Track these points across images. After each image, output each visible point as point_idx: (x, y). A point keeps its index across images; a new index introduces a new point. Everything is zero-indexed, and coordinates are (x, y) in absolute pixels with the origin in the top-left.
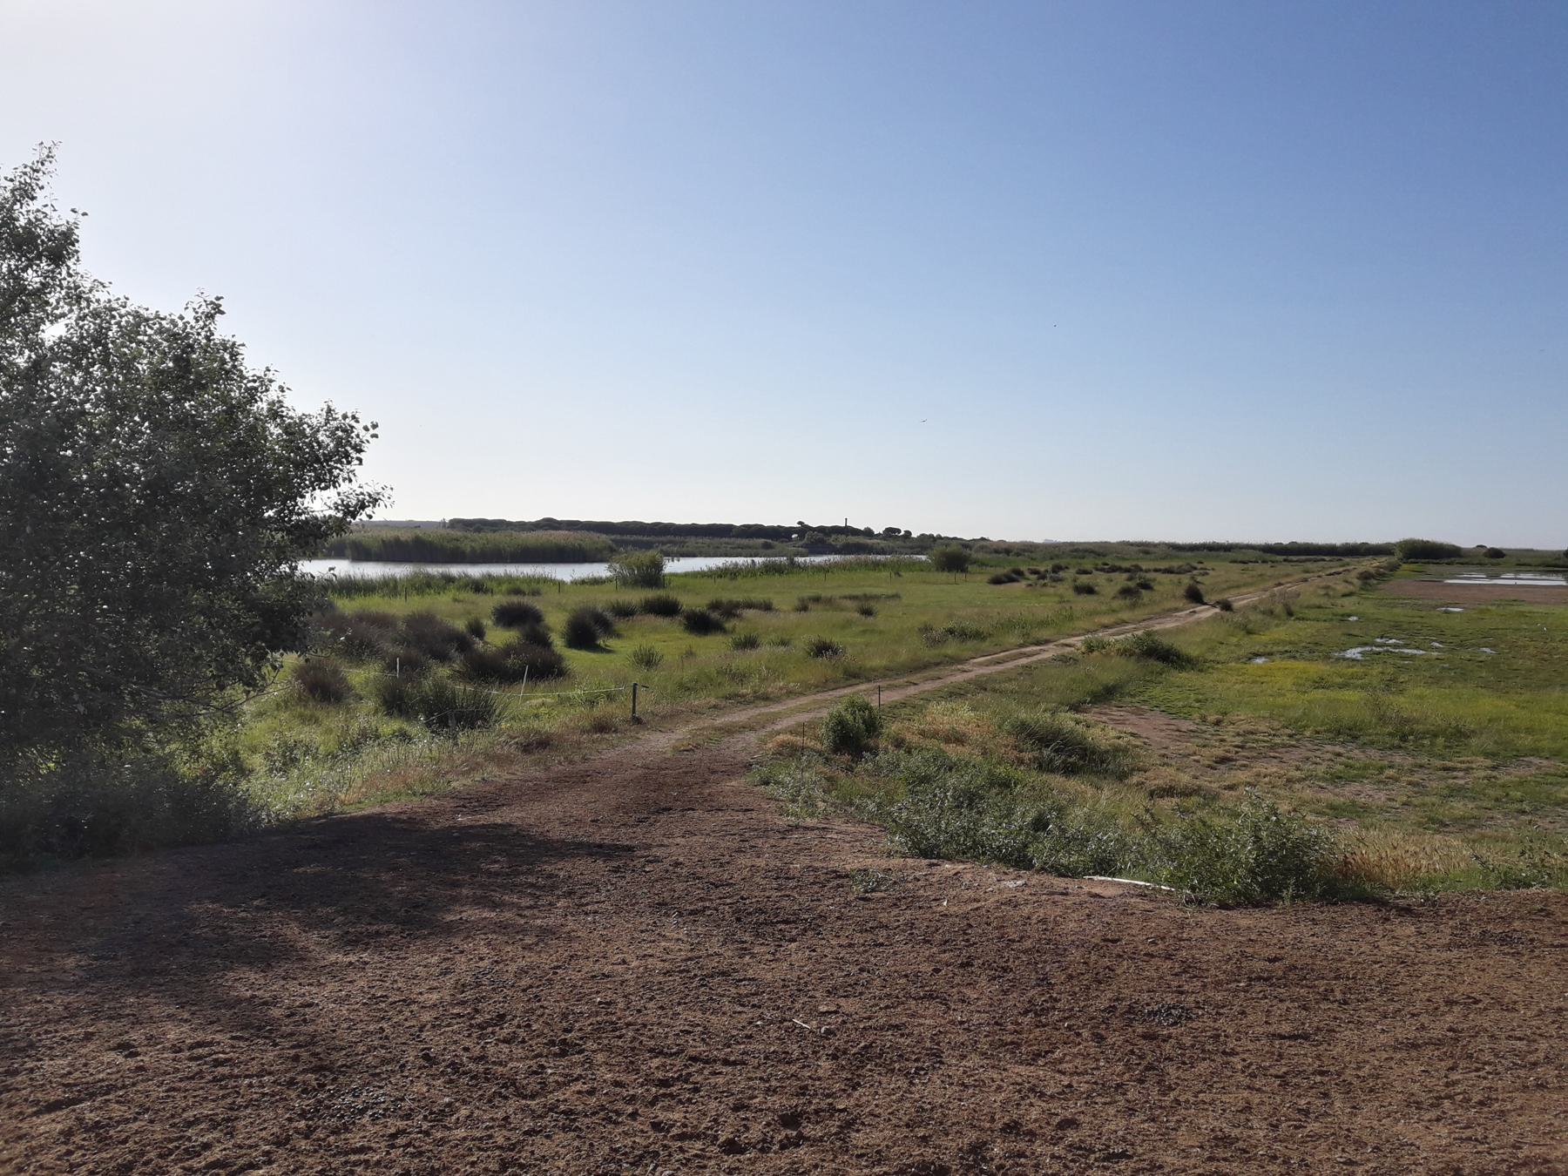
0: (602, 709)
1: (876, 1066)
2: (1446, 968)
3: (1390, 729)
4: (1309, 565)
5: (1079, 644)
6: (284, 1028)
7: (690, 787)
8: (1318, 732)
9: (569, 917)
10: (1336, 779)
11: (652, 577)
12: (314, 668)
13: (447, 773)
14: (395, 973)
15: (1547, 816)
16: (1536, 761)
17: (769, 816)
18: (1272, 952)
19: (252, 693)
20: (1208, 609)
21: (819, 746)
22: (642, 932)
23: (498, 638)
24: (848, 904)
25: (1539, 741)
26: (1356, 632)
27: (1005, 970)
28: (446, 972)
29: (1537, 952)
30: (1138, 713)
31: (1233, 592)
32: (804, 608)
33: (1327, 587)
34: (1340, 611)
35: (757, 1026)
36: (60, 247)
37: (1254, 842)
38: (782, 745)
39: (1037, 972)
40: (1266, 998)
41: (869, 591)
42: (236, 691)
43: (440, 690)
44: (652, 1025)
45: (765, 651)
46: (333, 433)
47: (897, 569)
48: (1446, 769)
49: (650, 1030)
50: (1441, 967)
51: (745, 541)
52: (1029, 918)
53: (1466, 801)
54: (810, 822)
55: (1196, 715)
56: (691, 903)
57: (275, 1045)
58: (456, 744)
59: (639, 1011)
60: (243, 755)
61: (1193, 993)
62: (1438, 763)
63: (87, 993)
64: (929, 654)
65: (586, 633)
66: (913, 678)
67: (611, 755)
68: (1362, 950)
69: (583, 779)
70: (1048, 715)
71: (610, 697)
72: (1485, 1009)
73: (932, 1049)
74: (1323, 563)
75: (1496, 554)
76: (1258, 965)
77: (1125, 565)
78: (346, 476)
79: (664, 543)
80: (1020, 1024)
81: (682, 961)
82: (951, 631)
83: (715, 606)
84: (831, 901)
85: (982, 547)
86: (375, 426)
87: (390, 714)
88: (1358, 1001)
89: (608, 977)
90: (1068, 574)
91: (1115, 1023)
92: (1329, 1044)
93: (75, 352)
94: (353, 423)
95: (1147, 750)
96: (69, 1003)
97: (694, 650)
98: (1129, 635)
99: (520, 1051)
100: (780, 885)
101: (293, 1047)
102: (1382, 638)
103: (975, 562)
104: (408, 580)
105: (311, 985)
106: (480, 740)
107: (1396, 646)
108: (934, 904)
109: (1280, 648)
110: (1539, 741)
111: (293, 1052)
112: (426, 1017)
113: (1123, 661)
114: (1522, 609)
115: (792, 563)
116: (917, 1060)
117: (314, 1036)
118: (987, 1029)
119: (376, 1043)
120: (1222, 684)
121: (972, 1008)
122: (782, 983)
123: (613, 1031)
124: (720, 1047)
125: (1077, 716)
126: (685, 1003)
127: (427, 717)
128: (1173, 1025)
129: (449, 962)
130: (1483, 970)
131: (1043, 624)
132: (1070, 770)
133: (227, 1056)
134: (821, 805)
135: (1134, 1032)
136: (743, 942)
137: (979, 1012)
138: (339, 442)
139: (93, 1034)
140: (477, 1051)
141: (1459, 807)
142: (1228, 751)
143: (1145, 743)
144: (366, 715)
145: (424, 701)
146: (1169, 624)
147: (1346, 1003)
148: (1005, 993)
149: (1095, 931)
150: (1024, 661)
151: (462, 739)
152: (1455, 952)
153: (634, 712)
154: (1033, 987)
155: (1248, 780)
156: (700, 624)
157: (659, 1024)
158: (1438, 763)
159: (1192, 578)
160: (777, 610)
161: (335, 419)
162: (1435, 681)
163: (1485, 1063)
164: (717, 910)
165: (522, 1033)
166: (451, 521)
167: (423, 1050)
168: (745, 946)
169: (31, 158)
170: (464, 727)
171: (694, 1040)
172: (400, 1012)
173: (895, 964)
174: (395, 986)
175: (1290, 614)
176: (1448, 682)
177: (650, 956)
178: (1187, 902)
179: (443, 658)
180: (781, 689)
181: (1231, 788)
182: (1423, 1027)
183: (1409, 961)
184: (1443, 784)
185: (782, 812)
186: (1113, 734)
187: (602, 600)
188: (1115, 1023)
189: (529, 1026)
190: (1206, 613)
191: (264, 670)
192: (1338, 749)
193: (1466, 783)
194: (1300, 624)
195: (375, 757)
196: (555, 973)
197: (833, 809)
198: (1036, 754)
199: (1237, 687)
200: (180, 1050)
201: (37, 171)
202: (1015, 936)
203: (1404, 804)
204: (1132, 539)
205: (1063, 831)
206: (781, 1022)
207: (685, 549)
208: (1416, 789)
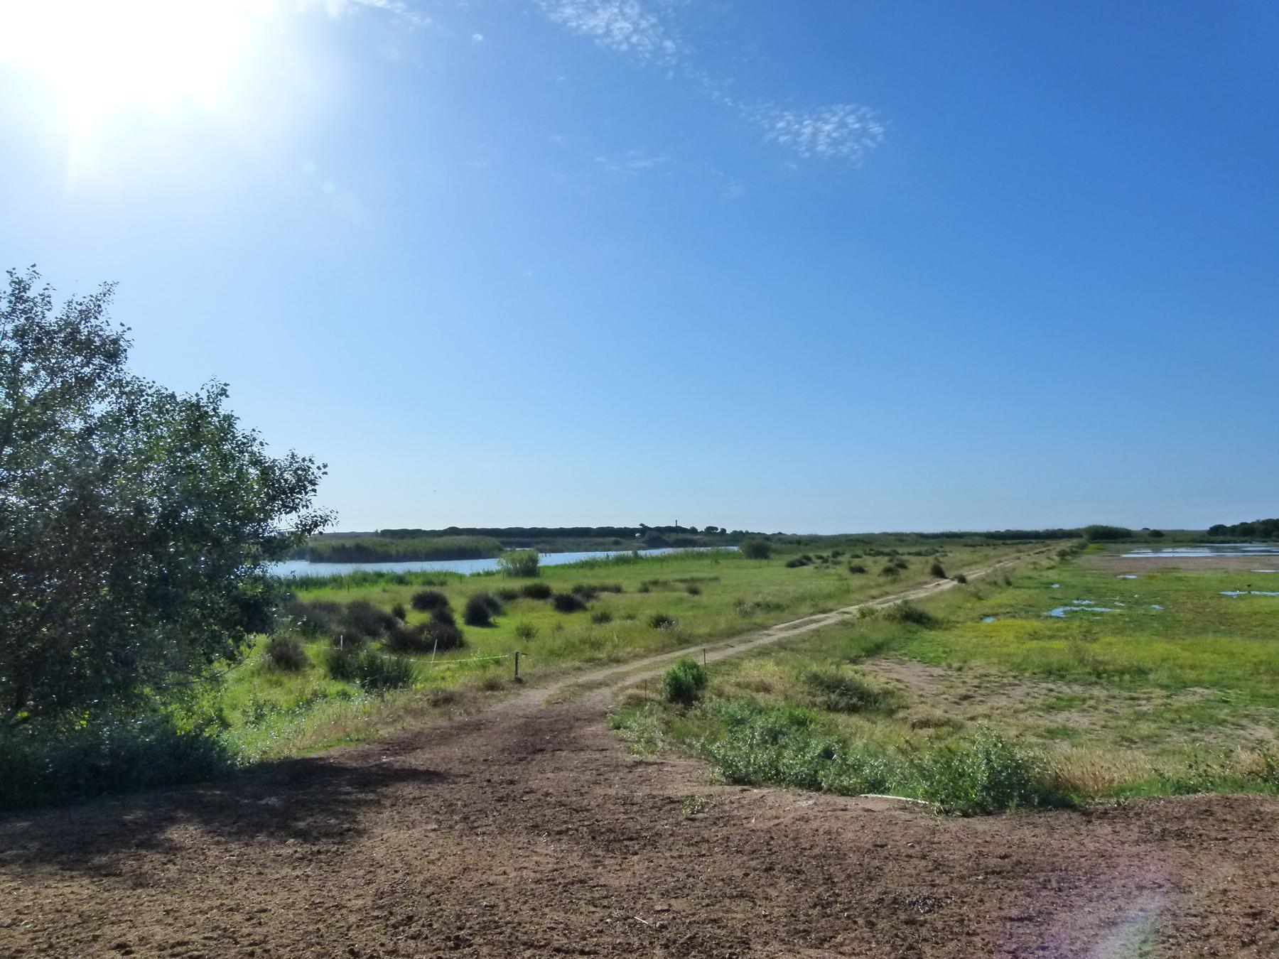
0: (492, 672)
1: (698, 952)
2: (1136, 859)
3: (1088, 669)
4: (1021, 547)
5: (855, 612)
6: (244, 929)
7: (560, 732)
8: (1035, 674)
9: (464, 838)
10: (1050, 708)
11: (530, 569)
12: (280, 644)
13: (376, 723)
14: (330, 883)
15: (1211, 733)
16: (1200, 690)
17: (619, 754)
18: (1002, 851)
19: (233, 666)
20: (947, 583)
21: (658, 698)
22: (519, 849)
23: (415, 618)
24: (678, 824)
25: (1201, 675)
26: (1059, 596)
27: (799, 872)
28: (369, 883)
29: (1205, 845)
30: (902, 663)
31: (967, 568)
32: (645, 590)
33: (1035, 563)
34: (1044, 580)
35: (607, 923)
36: (113, 351)
37: (987, 764)
38: (630, 697)
39: (823, 874)
40: (999, 888)
41: (695, 575)
42: (219, 666)
43: (372, 660)
44: (526, 923)
45: (616, 624)
46: (295, 472)
47: (716, 558)
48: (1132, 699)
49: (524, 927)
50: (1132, 859)
51: (600, 540)
52: (817, 830)
53: (1150, 723)
54: (651, 758)
55: (944, 664)
56: (557, 826)
57: (237, 943)
58: (383, 701)
59: (516, 912)
60: (226, 712)
61: (943, 885)
62: (1126, 694)
63: (97, 903)
64: (741, 623)
65: (481, 613)
66: (729, 642)
67: (498, 707)
68: (1072, 846)
69: (478, 727)
70: (834, 667)
71: (498, 662)
72: (1167, 892)
73: (741, 938)
74: (1030, 545)
75: (1157, 535)
76: (992, 862)
77: (886, 550)
78: (304, 504)
79: (538, 543)
80: (810, 916)
81: (550, 872)
82: (758, 605)
83: (578, 590)
84: (666, 822)
85: (780, 540)
86: (325, 466)
87: (335, 678)
88: (1070, 888)
89: (492, 885)
90: (844, 558)
91: (883, 912)
92: (1049, 925)
93: (111, 424)
94: (310, 464)
95: (908, 692)
96: (83, 912)
97: (562, 624)
98: (892, 604)
99: (423, 945)
100: (626, 810)
101: (250, 945)
102: (1078, 600)
103: (774, 551)
104: (350, 577)
105: (266, 894)
106: (398, 698)
107: (1088, 606)
108: (744, 821)
109: (1003, 610)
110: (1201, 675)
111: (250, 949)
112: (353, 919)
113: (887, 623)
114: (1180, 575)
115: (636, 554)
116: (731, 947)
117: (267, 936)
118: (785, 920)
119: (313, 941)
120: (961, 638)
121: (773, 904)
122: (627, 888)
123: (496, 928)
124: (578, 940)
125: (855, 667)
126: (551, 906)
127: (362, 680)
128: (927, 912)
129: (371, 874)
130: (1164, 861)
131: (829, 596)
132: (853, 710)
133: (200, 953)
134: (660, 744)
135: (898, 919)
136: (597, 856)
137: (779, 907)
138: (299, 480)
139: (98, 936)
140: (390, 946)
141: (1145, 728)
142: (969, 691)
143: (907, 686)
144: (317, 679)
145: (361, 668)
146: (921, 594)
147: (1060, 890)
148: (799, 890)
149: (867, 839)
150: (814, 626)
151: (387, 696)
152: (1143, 846)
153: (516, 673)
154: (820, 886)
155: (985, 712)
156: (567, 604)
157: (530, 922)
158: (1126, 694)
159: (936, 559)
160: (625, 592)
161: (297, 462)
162: (1119, 631)
163: (1170, 937)
164: (577, 830)
165: (426, 931)
166: (382, 531)
167: (349, 946)
168: (599, 859)
169: (96, 291)
170: (389, 687)
171: (558, 935)
172: (333, 915)
173: (714, 871)
174: (330, 894)
175: (1009, 583)
176: (1129, 632)
177: (525, 868)
178: (938, 813)
179: (374, 634)
180: (629, 653)
181: (973, 719)
182: (1120, 909)
183: (1107, 854)
184: (1131, 711)
185: (630, 751)
186: (883, 680)
187: (493, 587)
188: (883, 912)
189: (431, 925)
190: (947, 585)
191: (242, 648)
192: (1051, 686)
193: (1149, 709)
194: (1017, 592)
195: (324, 712)
196: (452, 883)
197: (669, 747)
198: (825, 698)
199: (974, 640)
200: (164, 949)
201: (99, 300)
202: (807, 846)
203: (1104, 727)
204: (890, 530)
205: (845, 760)
206: (625, 919)
207: (555, 547)
208: (1111, 715)
